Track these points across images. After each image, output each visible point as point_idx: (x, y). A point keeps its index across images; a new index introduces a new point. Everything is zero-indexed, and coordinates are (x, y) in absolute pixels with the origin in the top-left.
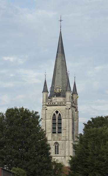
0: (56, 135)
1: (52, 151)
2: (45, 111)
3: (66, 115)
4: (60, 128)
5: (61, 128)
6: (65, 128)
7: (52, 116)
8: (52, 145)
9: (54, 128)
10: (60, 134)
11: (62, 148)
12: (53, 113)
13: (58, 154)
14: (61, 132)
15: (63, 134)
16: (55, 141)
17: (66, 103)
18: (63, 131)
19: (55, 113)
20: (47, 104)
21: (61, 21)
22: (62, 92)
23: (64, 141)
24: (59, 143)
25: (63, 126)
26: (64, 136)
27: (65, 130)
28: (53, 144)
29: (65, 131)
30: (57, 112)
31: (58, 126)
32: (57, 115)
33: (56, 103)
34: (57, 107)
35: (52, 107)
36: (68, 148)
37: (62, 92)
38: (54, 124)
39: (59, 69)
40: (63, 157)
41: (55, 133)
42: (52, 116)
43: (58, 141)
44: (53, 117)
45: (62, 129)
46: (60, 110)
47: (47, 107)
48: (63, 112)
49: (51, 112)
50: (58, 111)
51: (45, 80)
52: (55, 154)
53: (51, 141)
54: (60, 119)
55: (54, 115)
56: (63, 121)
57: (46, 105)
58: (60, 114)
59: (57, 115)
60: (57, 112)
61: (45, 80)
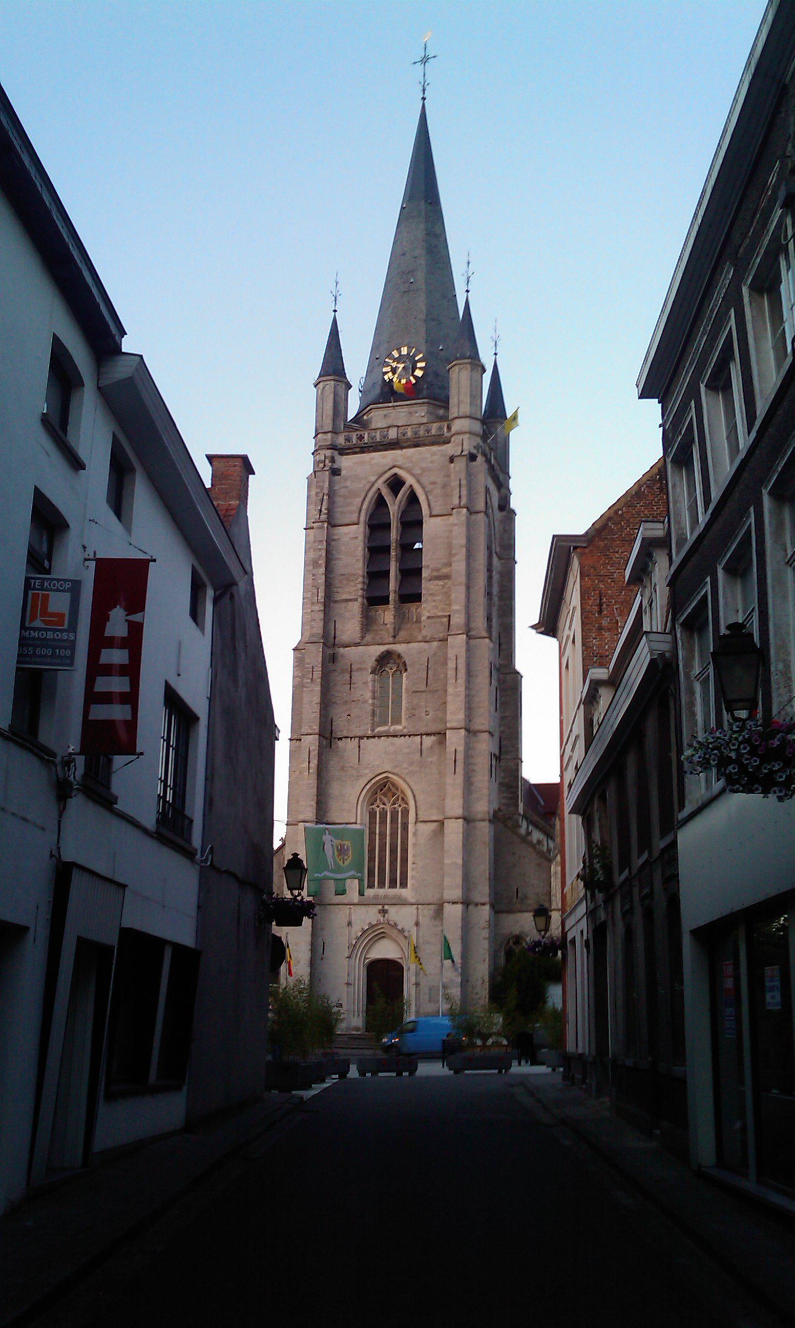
0: (387, 615)
1: (487, 997)
2: (482, 901)
3: (447, 496)
5: (419, 571)
6: (445, 571)
7: (365, 507)
8: (360, 669)
10: (413, 607)
11: (423, 688)
12: (374, 489)
13: (404, 885)
14: (416, 598)
15: (427, 608)
16: (383, 648)
17: (449, 428)
18: (427, 587)
19: (386, 493)
20: (341, 440)
21: (425, 60)
22: (429, 379)
23: (435, 644)
24: (406, 658)
25: (429, 563)
26: (432, 614)
27: (447, 577)
28: (371, 663)
29: (441, 583)
31: (401, 584)
32: (394, 507)
33: (393, 434)
34: (398, 452)
35: (366, 457)
36: (462, 680)
37: (429, 379)
39: (412, 271)
40: (428, 741)
41: (385, 601)
42: (365, 507)
43: (399, 648)
44: (372, 517)
45: (425, 573)
46: (417, 471)
47: (337, 457)
48: (433, 479)
49: (362, 485)
50: (402, 474)
51: (335, 321)
53: (357, 645)
55: (380, 502)
56: (431, 526)
57: (333, 447)
58: (413, 499)
59: (394, 507)
60: (396, 484)
61: (335, 321)
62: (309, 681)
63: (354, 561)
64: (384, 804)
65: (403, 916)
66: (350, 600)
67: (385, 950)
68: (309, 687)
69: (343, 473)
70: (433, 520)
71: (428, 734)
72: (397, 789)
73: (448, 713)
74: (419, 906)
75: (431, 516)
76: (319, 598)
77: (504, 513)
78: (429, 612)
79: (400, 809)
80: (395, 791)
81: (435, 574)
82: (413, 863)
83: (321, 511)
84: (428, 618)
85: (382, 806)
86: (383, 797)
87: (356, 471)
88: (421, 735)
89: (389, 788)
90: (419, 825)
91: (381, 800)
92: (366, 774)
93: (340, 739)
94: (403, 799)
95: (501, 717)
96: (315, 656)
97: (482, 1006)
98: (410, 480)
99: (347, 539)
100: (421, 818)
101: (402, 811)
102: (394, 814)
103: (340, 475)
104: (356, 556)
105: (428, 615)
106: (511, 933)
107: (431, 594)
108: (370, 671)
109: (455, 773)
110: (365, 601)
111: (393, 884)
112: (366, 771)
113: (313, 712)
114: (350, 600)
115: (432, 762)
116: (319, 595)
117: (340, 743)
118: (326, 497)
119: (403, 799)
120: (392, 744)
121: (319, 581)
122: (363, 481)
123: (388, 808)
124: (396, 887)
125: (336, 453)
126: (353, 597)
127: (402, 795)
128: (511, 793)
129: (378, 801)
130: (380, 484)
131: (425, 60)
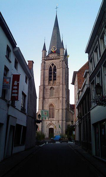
4: (55, 76)
9: (50, 77)
21: (57, 8)
28: (50, 88)
32: (53, 68)
38: (50, 73)
54: (55, 70)
58: (55, 66)
65: (54, 122)
67: (51, 127)
96: (42, 87)
98: (55, 64)
102: (53, 108)
111: (52, 118)
131: (57, 8)
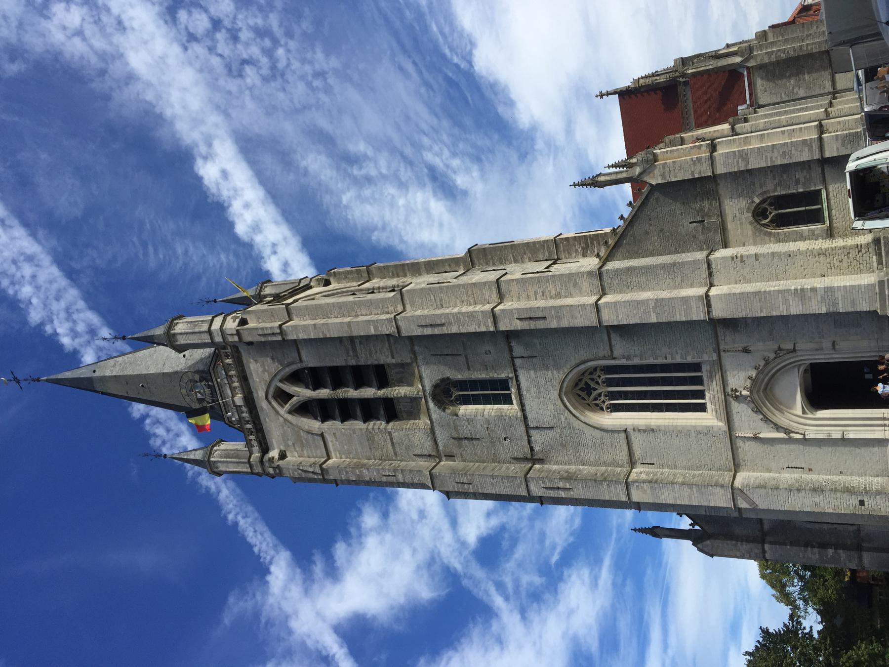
8: (456, 428)
12: (289, 417)
13: (697, 367)
16: (431, 405)
30: (283, 397)
32: (303, 393)
52: (508, 400)
62: (471, 486)
63: (355, 435)
64: (600, 395)
66: (391, 440)
68: (477, 486)
69: (282, 448)
70: (304, 358)
71: (511, 350)
72: (580, 380)
73: (478, 330)
74: (721, 347)
75: (301, 361)
76: (391, 474)
77: (332, 280)
78: (387, 357)
79: (603, 377)
80: (583, 382)
81: (351, 353)
82: (666, 358)
83: (313, 472)
84: (393, 357)
85: (602, 398)
86: (592, 397)
87: (279, 436)
88: (513, 358)
89: (586, 383)
90: (616, 354)
91: (596, 399)
92: (566, 419)
93: (532, 449)
94: (591, 373)
95: (515, 263)
97: (843, 145)
99: (337, 443)
100: (607, 352)
101: (605, 374)
102: (610, 383)
103: (285, 451)
104: (350, 434)
105: (390, 357)
106: (751, 223)
107: (371, 355)
108: (455, 417)
109: (544, 318)
110: (391, 424)
112: (563, 419)
113: (503, 483)
114: (391, 440)
115: (540, 344)
116: (387, 474)
117: (537, 448)
118: (301, 468)
119: (591, 373)
120: (528, 390)
121: (375, 474)
122: (285, 428)
123: (603, 389)
124: (701, 377)
125: (266, 458)
126: (388, 437)
127: (587, 374)
128: (592, 243)
129: (597, 402)
130: (283, 411)
